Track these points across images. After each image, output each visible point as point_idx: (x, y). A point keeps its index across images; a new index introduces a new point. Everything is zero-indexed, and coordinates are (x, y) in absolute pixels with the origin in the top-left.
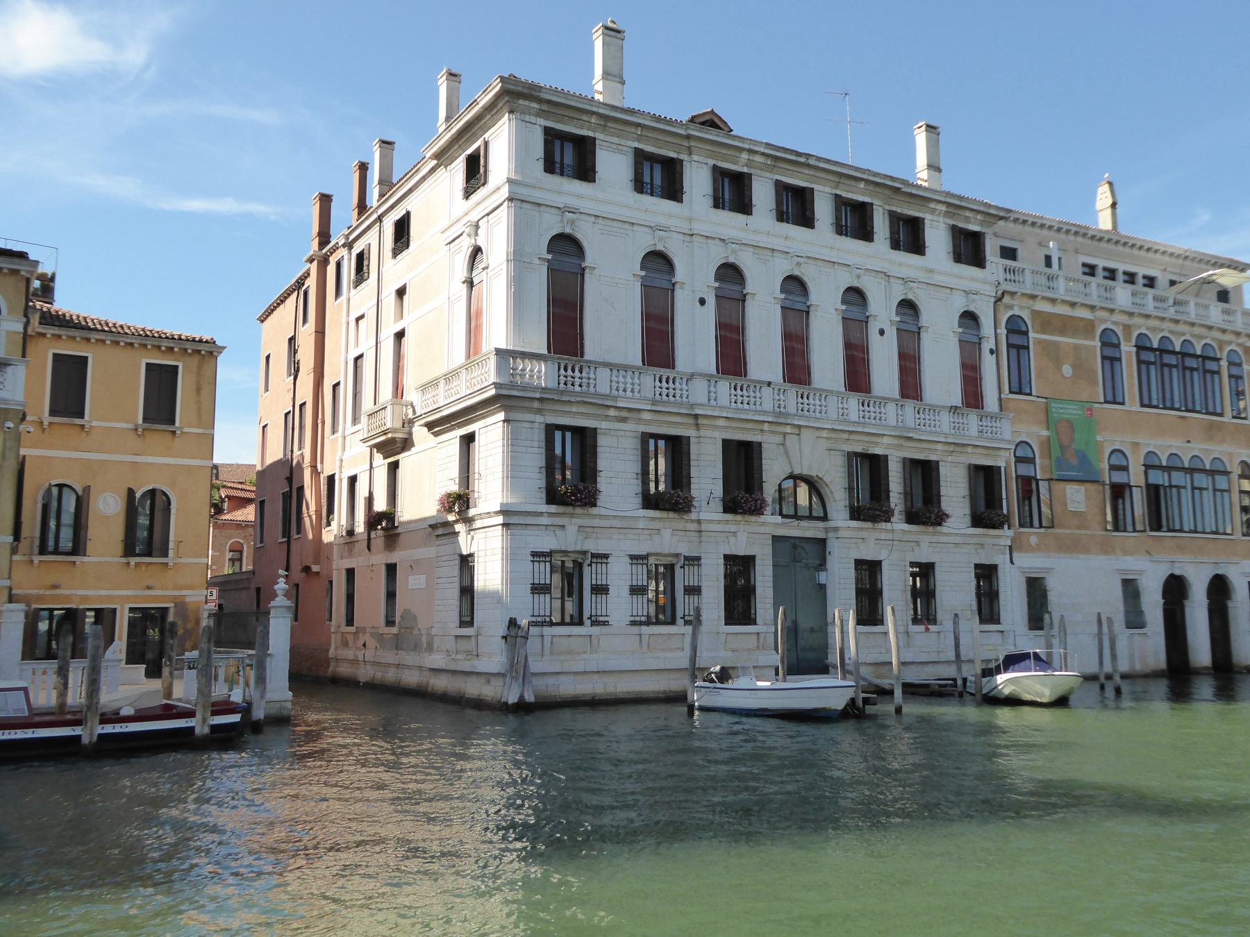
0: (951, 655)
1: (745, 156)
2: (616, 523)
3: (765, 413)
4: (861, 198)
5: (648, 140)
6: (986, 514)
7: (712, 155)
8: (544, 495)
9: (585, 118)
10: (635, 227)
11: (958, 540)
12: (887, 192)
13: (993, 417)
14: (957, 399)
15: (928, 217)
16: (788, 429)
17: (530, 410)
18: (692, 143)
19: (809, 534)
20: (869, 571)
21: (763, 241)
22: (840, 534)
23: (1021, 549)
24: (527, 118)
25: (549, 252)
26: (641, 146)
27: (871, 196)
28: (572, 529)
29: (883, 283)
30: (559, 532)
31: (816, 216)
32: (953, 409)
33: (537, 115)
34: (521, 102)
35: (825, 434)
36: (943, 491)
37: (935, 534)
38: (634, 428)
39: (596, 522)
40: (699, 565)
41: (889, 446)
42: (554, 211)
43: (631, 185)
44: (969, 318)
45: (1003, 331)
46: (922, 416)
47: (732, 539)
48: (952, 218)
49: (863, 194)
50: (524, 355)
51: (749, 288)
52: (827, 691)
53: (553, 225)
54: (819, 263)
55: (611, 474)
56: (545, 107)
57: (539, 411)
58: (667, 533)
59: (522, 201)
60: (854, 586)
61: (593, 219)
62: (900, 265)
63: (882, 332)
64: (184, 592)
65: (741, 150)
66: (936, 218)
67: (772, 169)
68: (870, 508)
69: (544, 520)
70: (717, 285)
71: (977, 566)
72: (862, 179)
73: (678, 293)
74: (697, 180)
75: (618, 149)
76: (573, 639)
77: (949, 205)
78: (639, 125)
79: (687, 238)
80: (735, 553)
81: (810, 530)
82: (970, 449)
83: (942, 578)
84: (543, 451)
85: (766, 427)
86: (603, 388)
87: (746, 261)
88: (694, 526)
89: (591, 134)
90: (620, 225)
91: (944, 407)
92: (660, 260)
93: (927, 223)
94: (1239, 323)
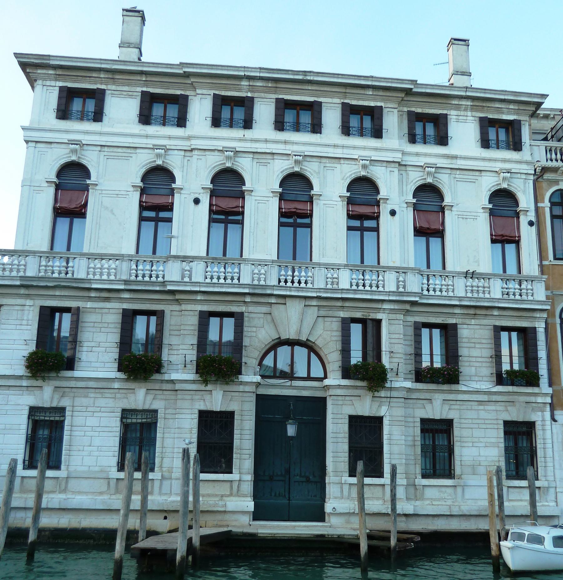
1: (245, 83)
3: (240, 285)
7: (212, 86)
8: (116, 365)
9: (94, 75)
11: (485, 398)
13: (531, 279)
15: (452, 114)
16: (273, 300)
18: (193, 80)
21: (261, 147)
24: (48, 83)
25: (490, 202)
33: (56, 80)
34: (39, 71)
37: (451, 392)
39: (73, 384)
42: (216, 153)
45: (546, 204)
54: (324, 160)
55: (93, 344)
56: (60, 72)
57: (28, 296)
59: (37, 142)
61: (99, 148)
62: (417, 154)
63: (393, 213)
67: (275, 90)
70: (490, 206)
71: (506, 423)
82: (496, 313)
85: (248, 299)
86: (81, 274)
91: (459, 273)
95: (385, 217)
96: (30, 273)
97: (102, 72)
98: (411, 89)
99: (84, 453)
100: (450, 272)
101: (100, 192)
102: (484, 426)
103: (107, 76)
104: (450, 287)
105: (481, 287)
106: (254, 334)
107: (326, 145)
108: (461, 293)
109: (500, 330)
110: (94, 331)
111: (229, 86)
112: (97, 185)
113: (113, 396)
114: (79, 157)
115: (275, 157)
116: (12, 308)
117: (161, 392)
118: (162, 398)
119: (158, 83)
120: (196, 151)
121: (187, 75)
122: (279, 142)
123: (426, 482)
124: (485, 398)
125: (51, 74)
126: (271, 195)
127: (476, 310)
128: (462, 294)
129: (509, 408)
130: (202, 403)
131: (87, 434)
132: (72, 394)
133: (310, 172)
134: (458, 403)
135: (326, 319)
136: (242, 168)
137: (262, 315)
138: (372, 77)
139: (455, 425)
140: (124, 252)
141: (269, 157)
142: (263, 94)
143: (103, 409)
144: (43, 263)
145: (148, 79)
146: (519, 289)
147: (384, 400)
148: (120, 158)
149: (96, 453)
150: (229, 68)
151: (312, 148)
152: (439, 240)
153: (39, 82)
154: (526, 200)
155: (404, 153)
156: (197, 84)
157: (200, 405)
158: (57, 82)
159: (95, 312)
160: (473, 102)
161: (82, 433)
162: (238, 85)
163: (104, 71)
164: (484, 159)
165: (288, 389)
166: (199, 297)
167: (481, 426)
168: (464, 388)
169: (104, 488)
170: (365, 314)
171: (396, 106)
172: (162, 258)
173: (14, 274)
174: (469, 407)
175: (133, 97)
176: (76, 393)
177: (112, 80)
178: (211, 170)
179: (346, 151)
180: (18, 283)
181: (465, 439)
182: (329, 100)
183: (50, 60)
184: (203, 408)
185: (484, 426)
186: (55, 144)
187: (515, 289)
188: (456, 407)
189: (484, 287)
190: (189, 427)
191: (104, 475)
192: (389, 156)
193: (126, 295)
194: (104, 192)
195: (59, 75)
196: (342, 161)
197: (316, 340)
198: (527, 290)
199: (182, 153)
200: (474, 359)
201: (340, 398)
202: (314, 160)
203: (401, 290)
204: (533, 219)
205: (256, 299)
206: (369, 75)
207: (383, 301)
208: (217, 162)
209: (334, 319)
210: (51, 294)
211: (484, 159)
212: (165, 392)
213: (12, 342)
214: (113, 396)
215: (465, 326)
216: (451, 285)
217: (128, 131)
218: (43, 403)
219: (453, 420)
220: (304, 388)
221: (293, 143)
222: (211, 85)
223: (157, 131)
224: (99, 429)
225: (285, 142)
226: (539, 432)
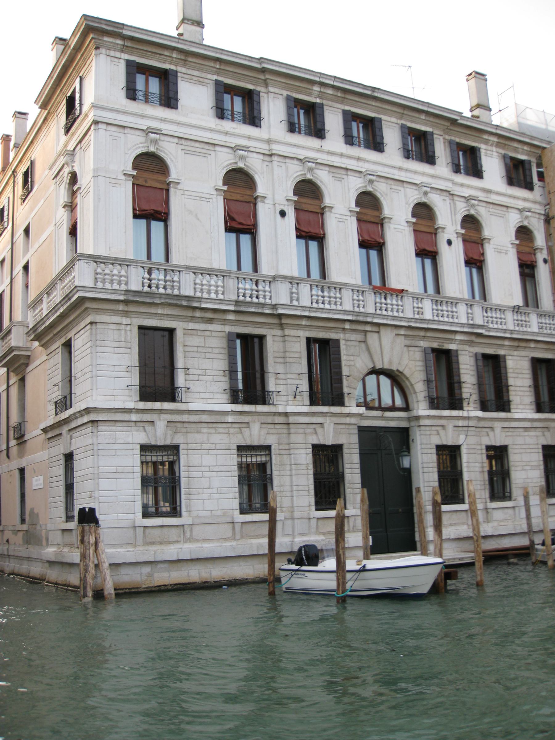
1: (316, 88)
2: (205, 418)
4: (423, 128)
7: (286, 87)
9: (166, 53)
10: (217, 148)
12: (448, 124)
14: (518, 300)
15: (483, 146)
16: (368, 328)
17: (116, 312)
18: (268, 76)
19: (392, 424)
20: (449, 455)
22: (423, 422)
24: (112, 53)
26: (220, 79)
27: (431, 126)
28: (161, 424)
29: (448, 201)
30: (149, 428)
32: (516, 309)
33: (122, 51)
34: (106, 39)
35: (402, 332)
36: (511, 382)
41: (462, 342)
42: (295, 162)
44: (524, 233)
46: (439, 308)
47: (319, 430)
48: (503, 148)
49: (425, 125)
51: (327, 201)
52: (411, 569)
55: (199, 372)
57: (126, 314)
58: (256, 427)
60: (436, 470)
61: (176, 140)
62: (462, 185)
63: (449, 242)
66: (489, 148)
67: (342, 101)
68: (448, 396)
69: (230, 419)
73: (261, 207)
75: (201, 82)
76: (165, 530)
79: (267, 158)
80: (445, 443)
81: (395, 420)
82: (532, 345)
83: (515, 459)
84: (226, 357)
85: (347, 326)
87: (323, 178)
88: (281, 419)
89: (173, 67)
90: (202, 145)
91: (509, 307)
93: (483, 152)
95: (443, 247)
96: (135, 286)
97: (175, 52)
98: (457, 120)
99: (205, 496)
100: (176, 266)
101: (182, 192)
103: (179, 57)
104: (123, 278)
105: (248, 289)
107: (393, 167)
109: (235, 337)
110: (199, 356)
111: (300, 89)
112: (179, 183)
113: (226, 431)
114: (157, 149)
115: (349, 173)
116: (106, 326)
117: (272, 426)
118: (275, 432)
119: (231, 73)
120: (276, 157)
121: (264, 71)
122: (352, 158)
125: (118, 44)
126: (349, 214)
127: (520, 343)
129: (546, 433)
130: (314, 437)
131: (206, 474)
132: (184, 430)
133: (380, 193)
134: (511, 430)
135: (411, 349)
136: (321, 182)
137: (357, 343)
138: (429, 103)
139: (510, 451)
140: (215, 266)
141: (343, 172)
143: (218, 446)
144: (355, 297)
145: (222, 67)
146: (149, 280)
147: (461, 429)
148: (197, 154)
149: (217, 496)
150: (306, 72)
151: (387, 170)
152: (162, 224)
153: (103, 50)
155: (454, 183)
156: (271, 81)
157: (313, 439)
158: (123, 54)
159: (197, 335)
160: (498, 139)
161: (200, 474)
162: (310, 89)
163: (177, 51)
164: (510, 196)
165: (377, 420)
166: (304, 322)
168: (517, 416)
169: (229, 534)
170: (440, 344)
171: (441, 133)
172: (268, 278)
173: (116, 286)
175: (204, 84)
176: (188, 429)
177: (183, 62)
178: (293, 181)
179: (409, 175)
180: (122, 298)
182: (388, 118)
183: (123, 29)
184: (316, 442)
185: (528, 451)
186: (129, 129)
187: (159, 280)
189: (202, 285)
190: (305, 462)
191: (229, 520)
192: (442, 185)
193: (231, 317)
194: (186, 193)
195: (127, 46)
196: (405, 185)
197: (404, 370)
198: (217, 287)
199: (261, 157)
200: (518, 389)
201: (427, 428)
202: (382, 180)
204: (546, 257)
205: (354, 327)
206: (426, 101)
207: (456, 332)
208: (297, 172)
209: (416, 349)
210: (153, 312)
211: (510, 196)
212: (277, 426)
213: (111, 368)
214: (226, 431)
216: (125, 277)
217: (204, 124)
218: (156, 440)
219: (179, 446)
220: (392, 419)
221: (365, 160)
222: (284, 84)
223: (234, 128)
224: (216, 469)
225: (359, 159)
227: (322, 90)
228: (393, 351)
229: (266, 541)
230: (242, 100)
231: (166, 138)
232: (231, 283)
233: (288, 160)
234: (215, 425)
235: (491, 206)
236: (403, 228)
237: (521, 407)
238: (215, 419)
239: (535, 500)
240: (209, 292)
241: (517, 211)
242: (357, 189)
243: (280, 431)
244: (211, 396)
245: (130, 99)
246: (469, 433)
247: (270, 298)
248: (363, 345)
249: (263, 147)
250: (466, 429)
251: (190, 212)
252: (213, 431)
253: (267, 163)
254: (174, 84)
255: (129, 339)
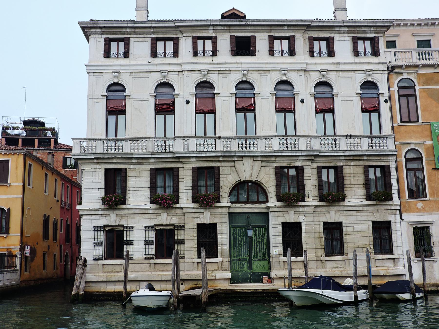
0: (366, 273)
1: (211, 28)
5: (158, 32)
6: (379, 193)
11: (360, 208)
13: (386, 137)
21: (223, 67)
23: (409, 211)
24: (97, 36)
30: (107, 217)
31: (257, 48)
33: (102, 34)
34: (92, 30)
37: (340, 206)
38: (148, 167)
39: (126, 212)
40: (183, 229)
42: (197, 72)
43: (268, 53)
50: (95, 140)
53: (109, 79)
62: (315, 64)
63: (302, 101)
64: (11, 247)
65: (208, 26)
69: (150, 211)
72: (284, 25)
74: (224, 44)
77: (348, 27)
78: (150, 27)
79: (181, 73)
85: (221, 159)
87: (213, 78)
88: (180, 211)
90: (144, 74)
92: (206, 85)
94: (437, 59)
98: (310, 25)
102: (360, 225)
106: (225, 179)
108: (344, 148)
113: (149, 217)
117: (175, 214)
123: (327, 258)
124: (360, 208)
126: (231, 95)
128: (345, 149)
132: (127, 218)
134: (345, 212)
135: (266, 168)
141: (228, 72)
142: (222, 34)
147: (301, 213)
154: (383, 88)
167: (358, 225)
171: (301, 34)
174: (351, 214)
179: (273, 65)
181: (349, 233)
185: (360, 225)
188: (345, 214)
194: (134, 100)
196: (271, 72)
200: (353, 186)
201: (276, 213)
202: (254, 72)
203: (309, 149)
204: (388, 99)
205: (225, 159)
209: (271, 167)
212: (177, 214)
215: (348, 167)
221: (241, 63)
226: (393, 227)
227: (215, 28)
228: (248, 171)
229: (123, 274)
230: (371, 43)
231: (376, 72)
232: (192, 143)
233: (192, 72)
234: (142, 215)
235: (341, 72)
236: (268, 98)
237: (355, 197)
238: (142, 212)
239: (361, 257)
240: (138, 149)
241: (363, 72)
242: (237, 80)
243: (179, 217)
244: (142, 200)
245: (356, 56)
246: (306, 215)
247: (336, 147)
248: (233, 168)
249: (179, 68)
250: (304, 212)
251: (136, 109)
252: (141, 218)
253: (181, 76)
254: (293, 44)
255: (100, 176)
